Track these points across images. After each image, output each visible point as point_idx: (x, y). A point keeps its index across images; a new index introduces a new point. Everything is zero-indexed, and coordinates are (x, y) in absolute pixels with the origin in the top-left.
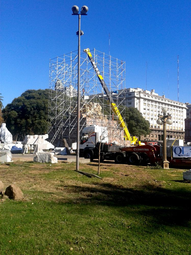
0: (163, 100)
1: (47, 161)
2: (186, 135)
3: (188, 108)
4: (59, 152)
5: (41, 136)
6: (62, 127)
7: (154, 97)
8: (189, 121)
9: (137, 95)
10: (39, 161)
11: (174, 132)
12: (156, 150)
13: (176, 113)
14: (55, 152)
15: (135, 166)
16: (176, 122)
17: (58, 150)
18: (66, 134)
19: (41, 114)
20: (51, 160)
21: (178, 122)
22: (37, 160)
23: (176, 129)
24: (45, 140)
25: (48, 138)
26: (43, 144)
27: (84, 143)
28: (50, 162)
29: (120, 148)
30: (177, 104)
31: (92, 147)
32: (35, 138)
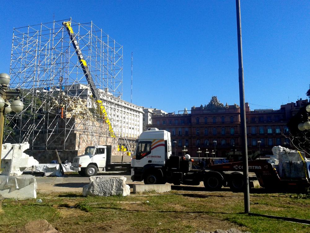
0: (119, 101)
1: (114, 192)
3: (144, 113)
4: (52, 173)
5: (17, 145)
6: (33, 131)
7: (109, 98)
9: (90, 93)
10: (96, 193)
11: (130, 140)
12: (229, 167)
13: (133, 117)
14: (46, 172)
15: (264, 194)
16: (132, 128)
17: (51, 168)
18: (39, 142)
20: (122, 190)
21: (135, 129)
22: (93, 191)
23: (132, 136)
24: (24, 152)
25: (29, 148)
26: (20, 158)
27: (143, 157)
28: (119, 195)
29: (123, 163)
30: (134, 107)
31: (159, 163)
32: (7, 148)
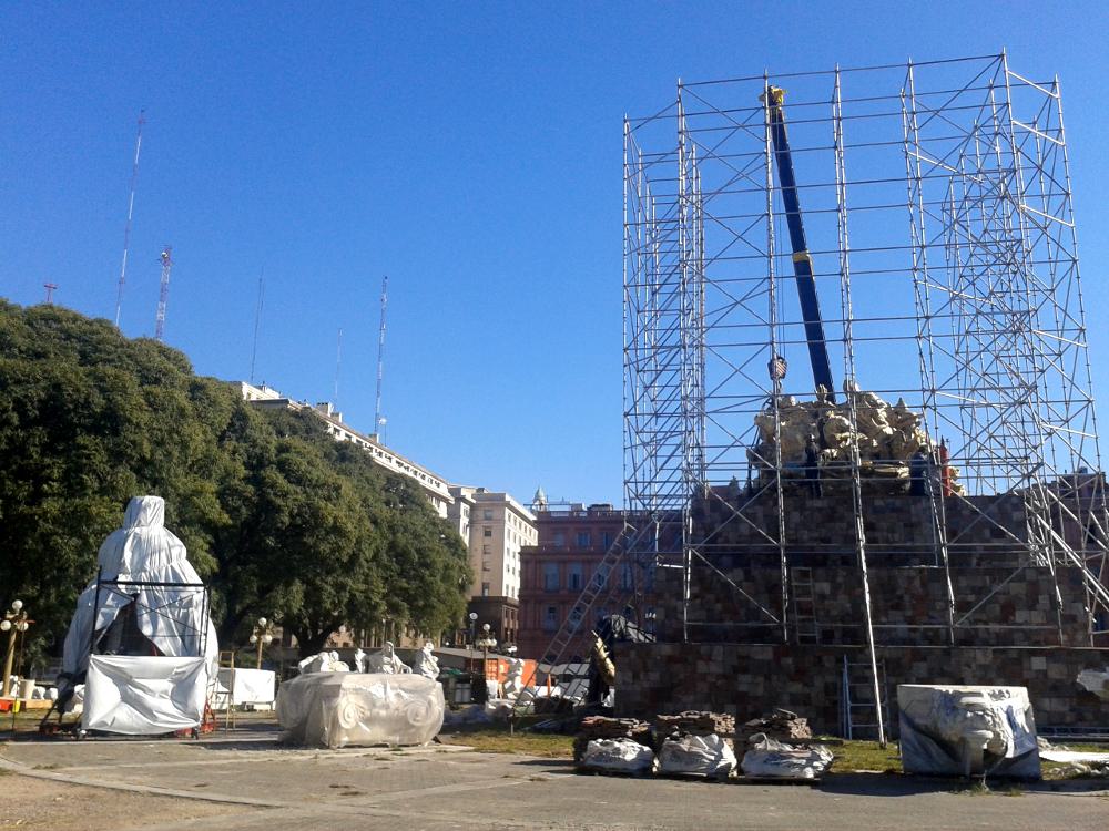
2: (525, 624)
8: (542, 558)
19: (88, 457)
30: (423, 477)
